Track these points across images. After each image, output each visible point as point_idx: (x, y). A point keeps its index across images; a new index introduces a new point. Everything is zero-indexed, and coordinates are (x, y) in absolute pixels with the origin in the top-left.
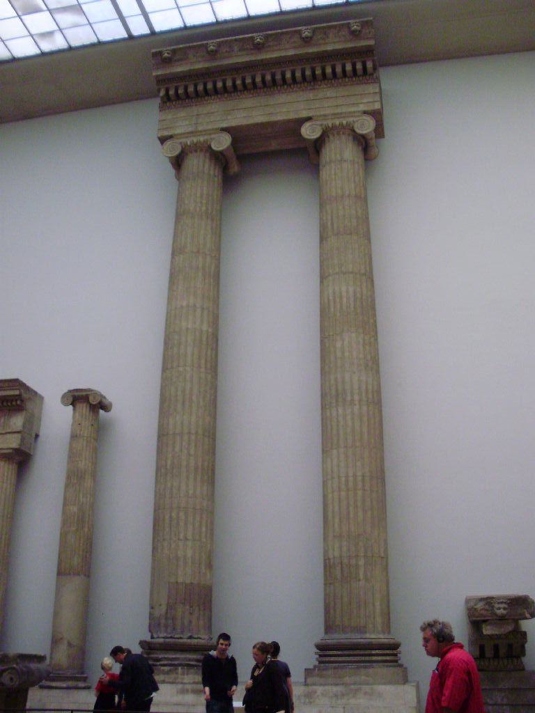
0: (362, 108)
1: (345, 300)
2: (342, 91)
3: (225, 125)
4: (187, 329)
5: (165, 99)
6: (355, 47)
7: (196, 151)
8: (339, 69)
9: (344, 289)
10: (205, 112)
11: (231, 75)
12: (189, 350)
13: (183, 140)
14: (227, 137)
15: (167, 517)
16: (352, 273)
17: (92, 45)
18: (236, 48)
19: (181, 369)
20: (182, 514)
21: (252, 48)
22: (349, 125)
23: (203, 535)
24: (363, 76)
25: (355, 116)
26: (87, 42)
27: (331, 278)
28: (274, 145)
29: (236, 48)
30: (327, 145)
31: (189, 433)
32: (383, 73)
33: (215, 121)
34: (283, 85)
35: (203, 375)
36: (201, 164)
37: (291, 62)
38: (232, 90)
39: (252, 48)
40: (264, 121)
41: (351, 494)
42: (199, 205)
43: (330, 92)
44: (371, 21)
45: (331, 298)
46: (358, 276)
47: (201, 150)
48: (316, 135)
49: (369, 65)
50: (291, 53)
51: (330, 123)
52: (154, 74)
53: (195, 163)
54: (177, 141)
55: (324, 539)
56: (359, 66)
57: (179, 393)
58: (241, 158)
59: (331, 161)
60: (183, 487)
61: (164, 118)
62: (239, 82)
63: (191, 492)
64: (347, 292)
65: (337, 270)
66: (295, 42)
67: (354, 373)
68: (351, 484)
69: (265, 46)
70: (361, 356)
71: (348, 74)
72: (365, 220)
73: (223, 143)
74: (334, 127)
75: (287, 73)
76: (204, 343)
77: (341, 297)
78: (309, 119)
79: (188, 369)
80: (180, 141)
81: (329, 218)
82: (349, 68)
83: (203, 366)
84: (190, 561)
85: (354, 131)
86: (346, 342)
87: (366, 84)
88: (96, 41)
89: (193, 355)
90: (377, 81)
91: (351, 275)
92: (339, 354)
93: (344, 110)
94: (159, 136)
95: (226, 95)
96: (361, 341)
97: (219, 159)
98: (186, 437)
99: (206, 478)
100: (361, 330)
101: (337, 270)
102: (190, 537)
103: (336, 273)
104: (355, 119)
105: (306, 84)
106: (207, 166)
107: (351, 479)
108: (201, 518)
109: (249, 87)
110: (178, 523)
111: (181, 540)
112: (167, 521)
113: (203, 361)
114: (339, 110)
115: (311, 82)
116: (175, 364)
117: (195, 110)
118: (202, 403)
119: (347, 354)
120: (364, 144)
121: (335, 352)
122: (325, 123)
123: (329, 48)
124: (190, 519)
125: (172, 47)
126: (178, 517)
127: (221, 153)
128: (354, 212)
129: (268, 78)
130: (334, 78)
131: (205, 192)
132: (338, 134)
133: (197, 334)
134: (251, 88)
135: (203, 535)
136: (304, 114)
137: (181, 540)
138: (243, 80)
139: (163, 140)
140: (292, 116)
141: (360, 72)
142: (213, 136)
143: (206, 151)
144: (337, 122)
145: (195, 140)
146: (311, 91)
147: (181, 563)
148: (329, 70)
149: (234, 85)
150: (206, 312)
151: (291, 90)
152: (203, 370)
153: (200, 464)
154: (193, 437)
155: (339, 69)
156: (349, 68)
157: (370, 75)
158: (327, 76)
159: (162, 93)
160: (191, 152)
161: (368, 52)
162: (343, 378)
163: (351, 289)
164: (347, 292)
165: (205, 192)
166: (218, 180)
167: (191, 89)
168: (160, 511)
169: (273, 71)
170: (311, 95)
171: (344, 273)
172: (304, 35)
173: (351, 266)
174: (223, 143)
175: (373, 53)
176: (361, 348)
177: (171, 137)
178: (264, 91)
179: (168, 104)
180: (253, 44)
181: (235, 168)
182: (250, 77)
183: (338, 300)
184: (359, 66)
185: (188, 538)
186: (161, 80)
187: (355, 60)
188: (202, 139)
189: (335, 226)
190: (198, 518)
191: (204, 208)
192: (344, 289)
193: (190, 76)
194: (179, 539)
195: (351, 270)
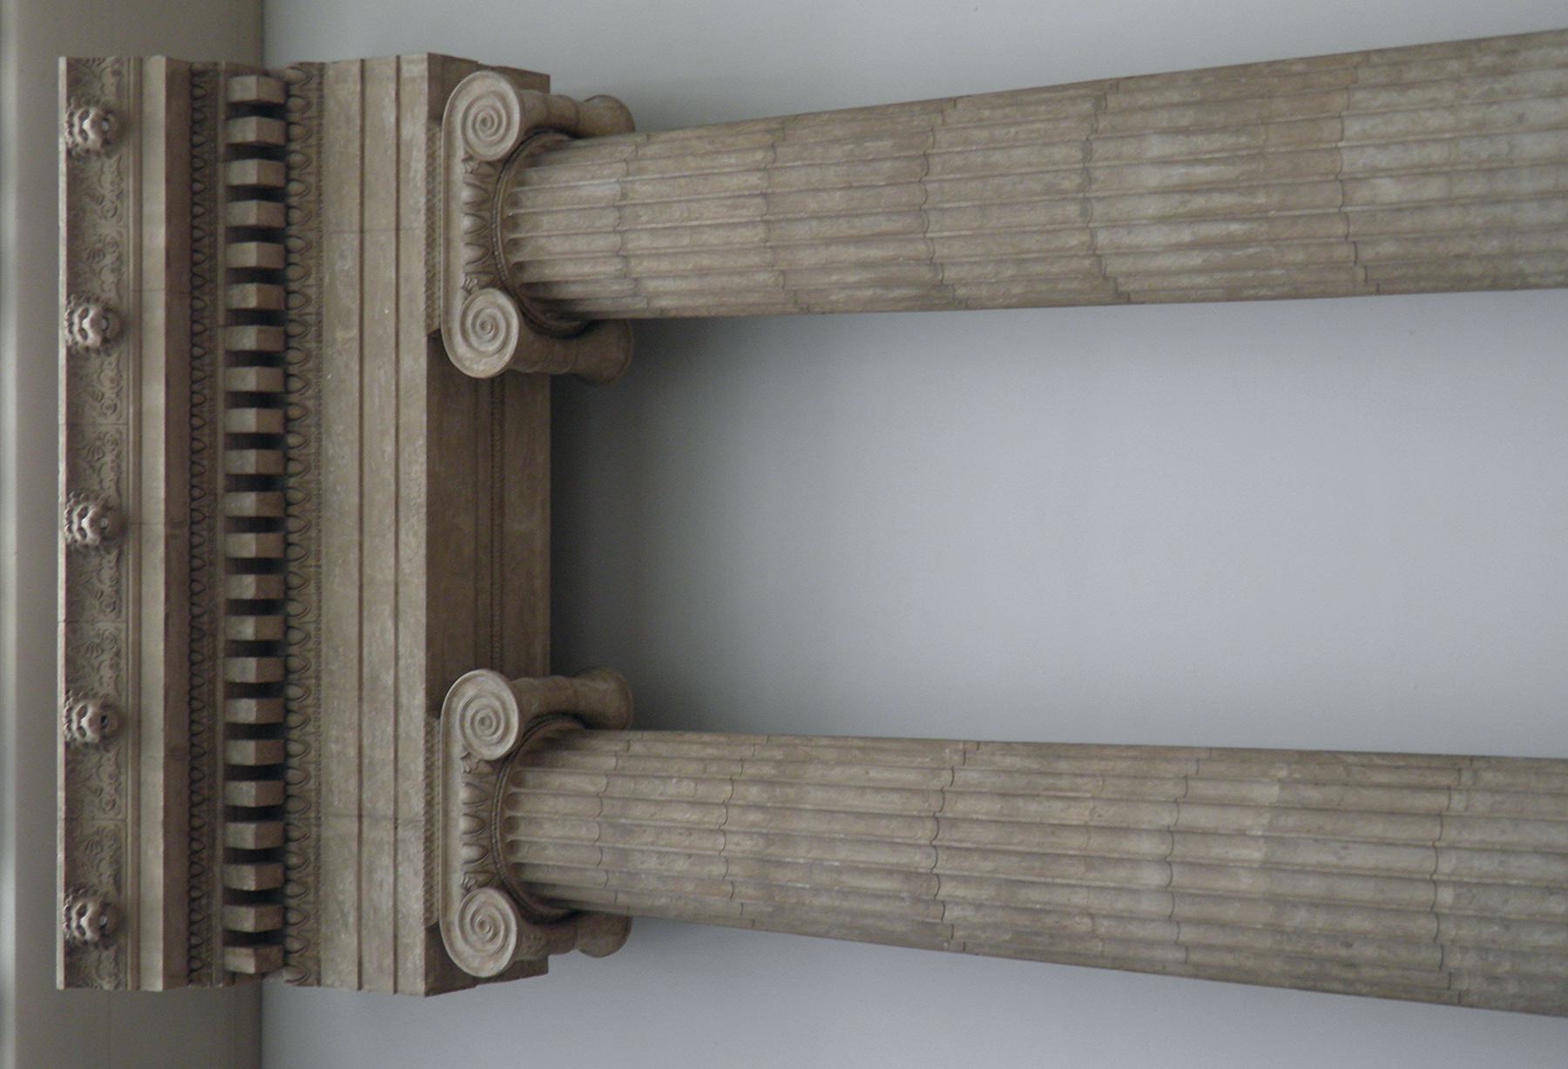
0: (416, 128)
1: (1202, 172)
2: (341, 209)
3: (416, 699)
4: (1269, 867)
5: (274, 952)
6: (166, 824)
7: (510, 825)
8: (250, 213)
9: (1152, 177)
10: (352, 784)
11: (213, 658)
12: (1360, 858)
13: (458, 878)
14: (470, 691)
16: (1088, 154)
21: (113, 556)
22: (481, 776)
24: (286, 909)
25: (449, 156)
27: (1103, 238)
28: (529, 523)
29: (106, 625)
30: (550, 273)
32: (288, 53)
33: (394, 721)
35: (1482, 802)
36: (561, 804)
37: (193, 858)
38: (272, 496)
39: (112, 952)
40: (422, 529)
42: (734, 813)
43: (341, 262)
44: (71, 66)
45: (1186, 235)
46: (1103, 123)
47: (511, 801)
48: (501, 308)
49: (247, 89)
50: (156, 396)
51: (464, 254)
52: (159, 986)
53: (565, 826)
54: (457, 905)
56: (249, 130)
58: (565, 657)
59: (621, 254)
61: (348, 968)
62: (248, 629)
64: (1165, 162)
65: (1072, 210)
66: (117, 381)
67: (1521, 118)
69: (113, 502)
70: (1448, 94)
71: (272, 345)
72: (871, 119)
73: (490, 706)
74: (482, 237)
75: (236, 513)
76: (1333, 793)
77: (1190, 189)
78: (436, 343)
79: (1447, 864)
80: (456, 891)
81: (851, 253)
82: (248, 172)
83: (1441, 801)
85: (508, 160)
86: (1382, 159)
87: (320, 115)
90: (314, 74)
91: (1100, 149)
92: (1433, 189)
93: (416, 198)
94: (421, 986)
96: (1384, 98)
97: (551, 735)
100: (1339, 101)
101: (1072, 210)
103: (1085, 213)
104: (460, 153)
105: (293, 356)
106: (572, 782)
109: (271, 922)
113: (1422, 801)
114: (416, 224)
115: (288, 336)
116: (1423, 926)
117: (338, 829)
119: (1436, 154)
120: (568, 725)
121: (1422, 207)
122: (460, 279)
123: (157, 237)
125: (61, 895)
127: (530, 725)
128: (837, 152)
129: (248, 504)
130: (286, 238)
131: (687, 788)
133: (1290, 821)
134: (282, 583)
136: (416, 363)
138: (240, 898)
139: (445, 976)
140: (417, 415)
141: (272, 586)
142: (457, 750)
143: (518, 781)
144: (464, 223)
145: (462, 824)
146: (326, 336)
148: (250, 254)
149: (261, 648)
150: (1202, 789)
151: (310, 421)
152: (1458, 802)
155: (250, 213)
156: (248, 172)
157: (288, 96)
158: (269, 802)
159: (244, 961)
160: (513, 846)
161: (195, 91)
162: (1536, 164)
163: (1157, 147)
164: (1165, 162)
165: (687, 788)
166: (641, 743)
167: (246, 835)
170: (342, 336)
171: (1089, 180)
172: (93, 338)
173: (1059, 153)
174: (490, 706)
175: (202, 73)
176: (1415, 95)
177: (434, 934)
178: (301, 252)
179: (295, 945)
180: (97, 747)
181: (600, 691)
182: (234, 454)
183: (1198, 202)
184: (249, 130)
186: (190, 963)
187: (221, 149)
188: (462, 794)
189: (885, 225)
191: (754, 793)
192: (1152, 177)
193: (192, 833)
195: (1077, 154)
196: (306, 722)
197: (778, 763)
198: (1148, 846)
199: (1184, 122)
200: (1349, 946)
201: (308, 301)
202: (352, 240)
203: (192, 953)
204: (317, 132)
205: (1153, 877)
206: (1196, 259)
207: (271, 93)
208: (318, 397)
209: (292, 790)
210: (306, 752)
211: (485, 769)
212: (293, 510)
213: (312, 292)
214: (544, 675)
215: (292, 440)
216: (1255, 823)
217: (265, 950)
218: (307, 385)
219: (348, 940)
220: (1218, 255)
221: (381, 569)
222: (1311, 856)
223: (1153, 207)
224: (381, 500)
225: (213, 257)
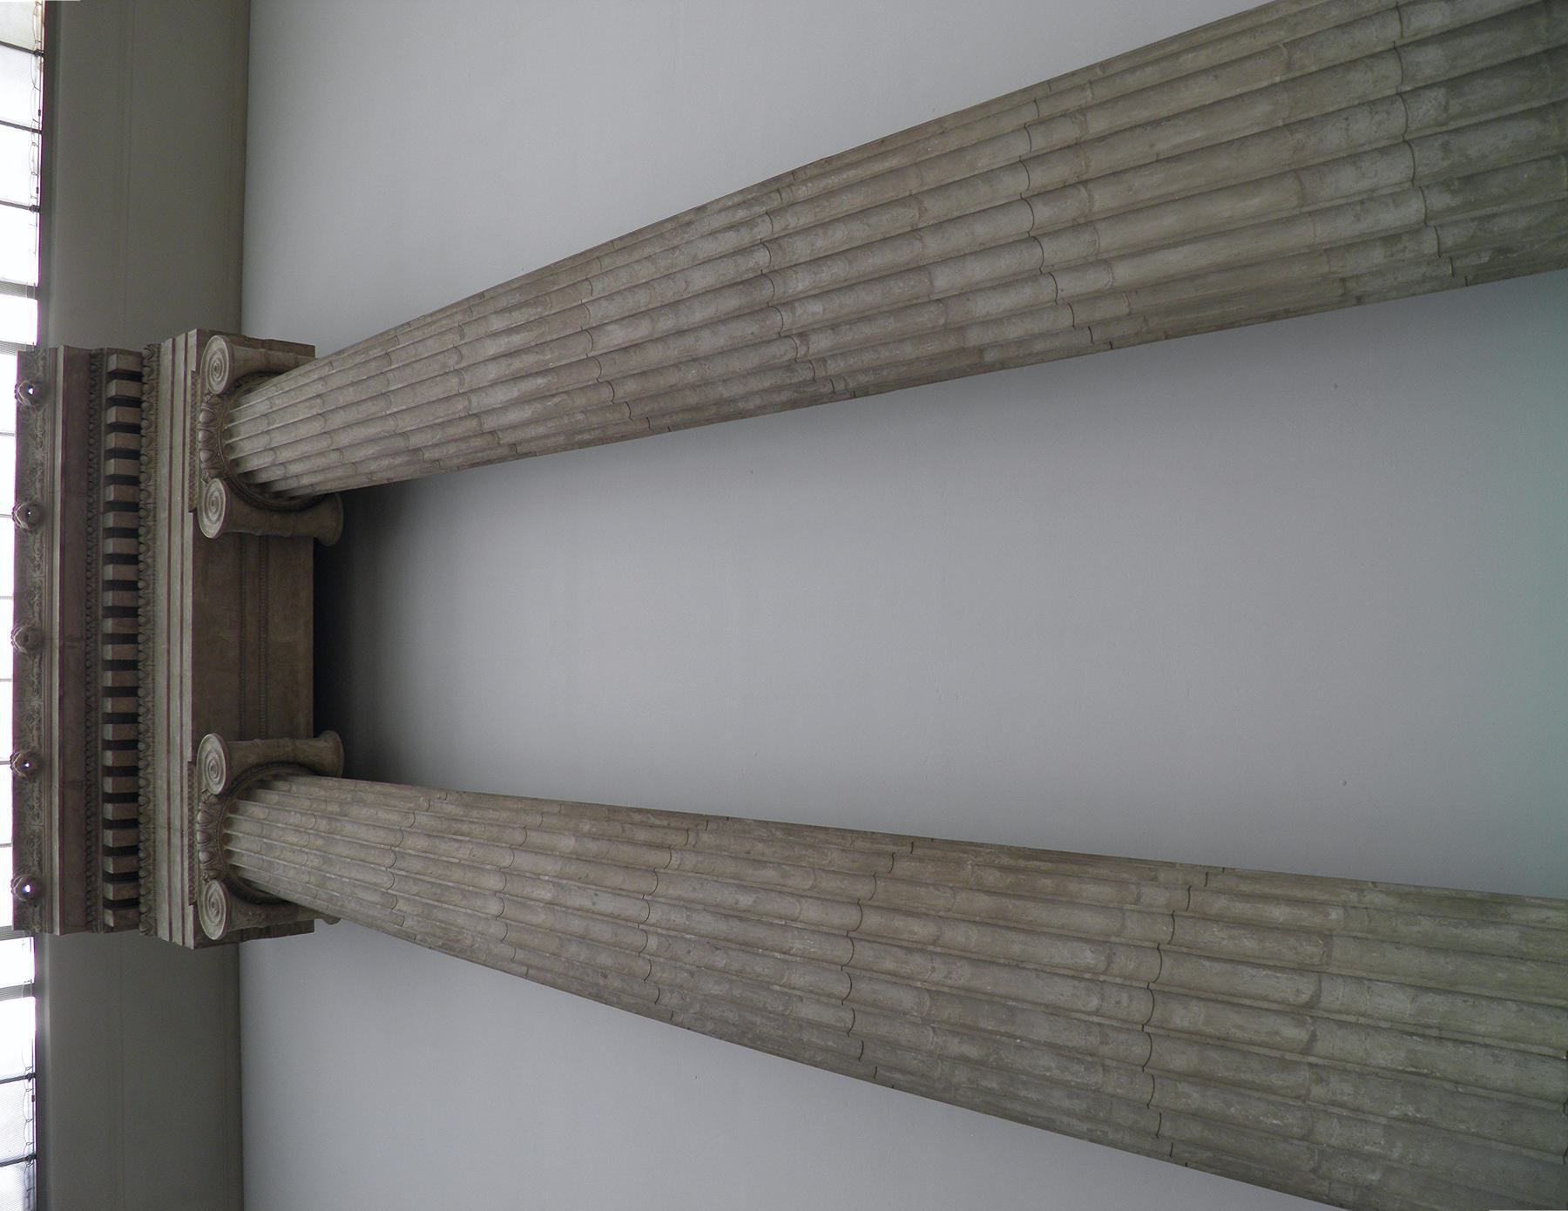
5: (131, 913)
7: (227, 839)
12: (606, 904)
15: (1194, 1097)
17: (39, 1098)
18: (36, 703)
19: (653, 943)
20: (1183, 1016)
22: (212, 804)
23: (1306, 916)
26: (28, 1109)
29: (36, 703)
31: (851, 935)
34: (137, 589)
41: (1100, 160)
47: (228, 823)
55: (1232, 325)
57: (720, 960)
60: (1060, 992)
63: (1088, 957)
68: (1060, 171)
84: (1438, 1004)
88: (30, 1084)
89: (617, 892)
95: (141, 746)
98: (866, 953)
99: (1047, 883)
102: (1303, 989)
107: (1041, 177)
108: (1218, 919)
110: (1223, 1043)
111: (1313, 1037)
112: (1212, 1102)
118: (770, 874)
124: (1214, 976)
126: (1192, 1037)
132: (236, 462)
135: (1306, 916)
137: (1313, 1037)
147: (1444, 1059)
153: (983, 902)
154: (873, 921)
168: (1167, 1129)
169: (100, 612)
185: (1304, 998)
190: (1216, 936)
194: (1307, 1049)
196: (148, 765)
197: (341, 804)
198: (494, 882)
199: (515, 301)
200: (605, 976)
201: (149, 495)
202: (167, 453)
203: (88, 910)
204: (155, 388)
205: (494, 907)
206: (526, 413)
207: (129, 364)
208: (154, 557)
209: (141, 809)
210: (148, 785)
211: (213, 800)
212: (141, 630)
213: (151, 489)
214: (308, 737)
215: (140, 584)
216: (549, 866)
217: (123, 912)
218: (148, 549)
219: (165, 907)
220: (538, 407)
221: (176, 670)
222: (579, 900)
223: (493, 371)
224: (176, 620)
225: (98, 470)
